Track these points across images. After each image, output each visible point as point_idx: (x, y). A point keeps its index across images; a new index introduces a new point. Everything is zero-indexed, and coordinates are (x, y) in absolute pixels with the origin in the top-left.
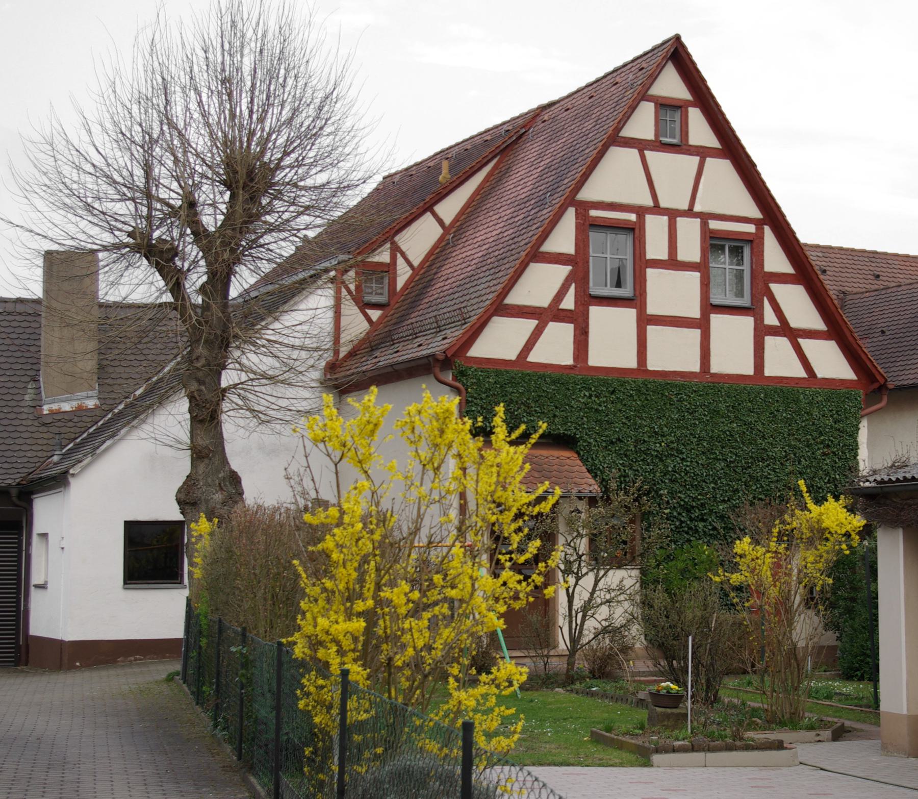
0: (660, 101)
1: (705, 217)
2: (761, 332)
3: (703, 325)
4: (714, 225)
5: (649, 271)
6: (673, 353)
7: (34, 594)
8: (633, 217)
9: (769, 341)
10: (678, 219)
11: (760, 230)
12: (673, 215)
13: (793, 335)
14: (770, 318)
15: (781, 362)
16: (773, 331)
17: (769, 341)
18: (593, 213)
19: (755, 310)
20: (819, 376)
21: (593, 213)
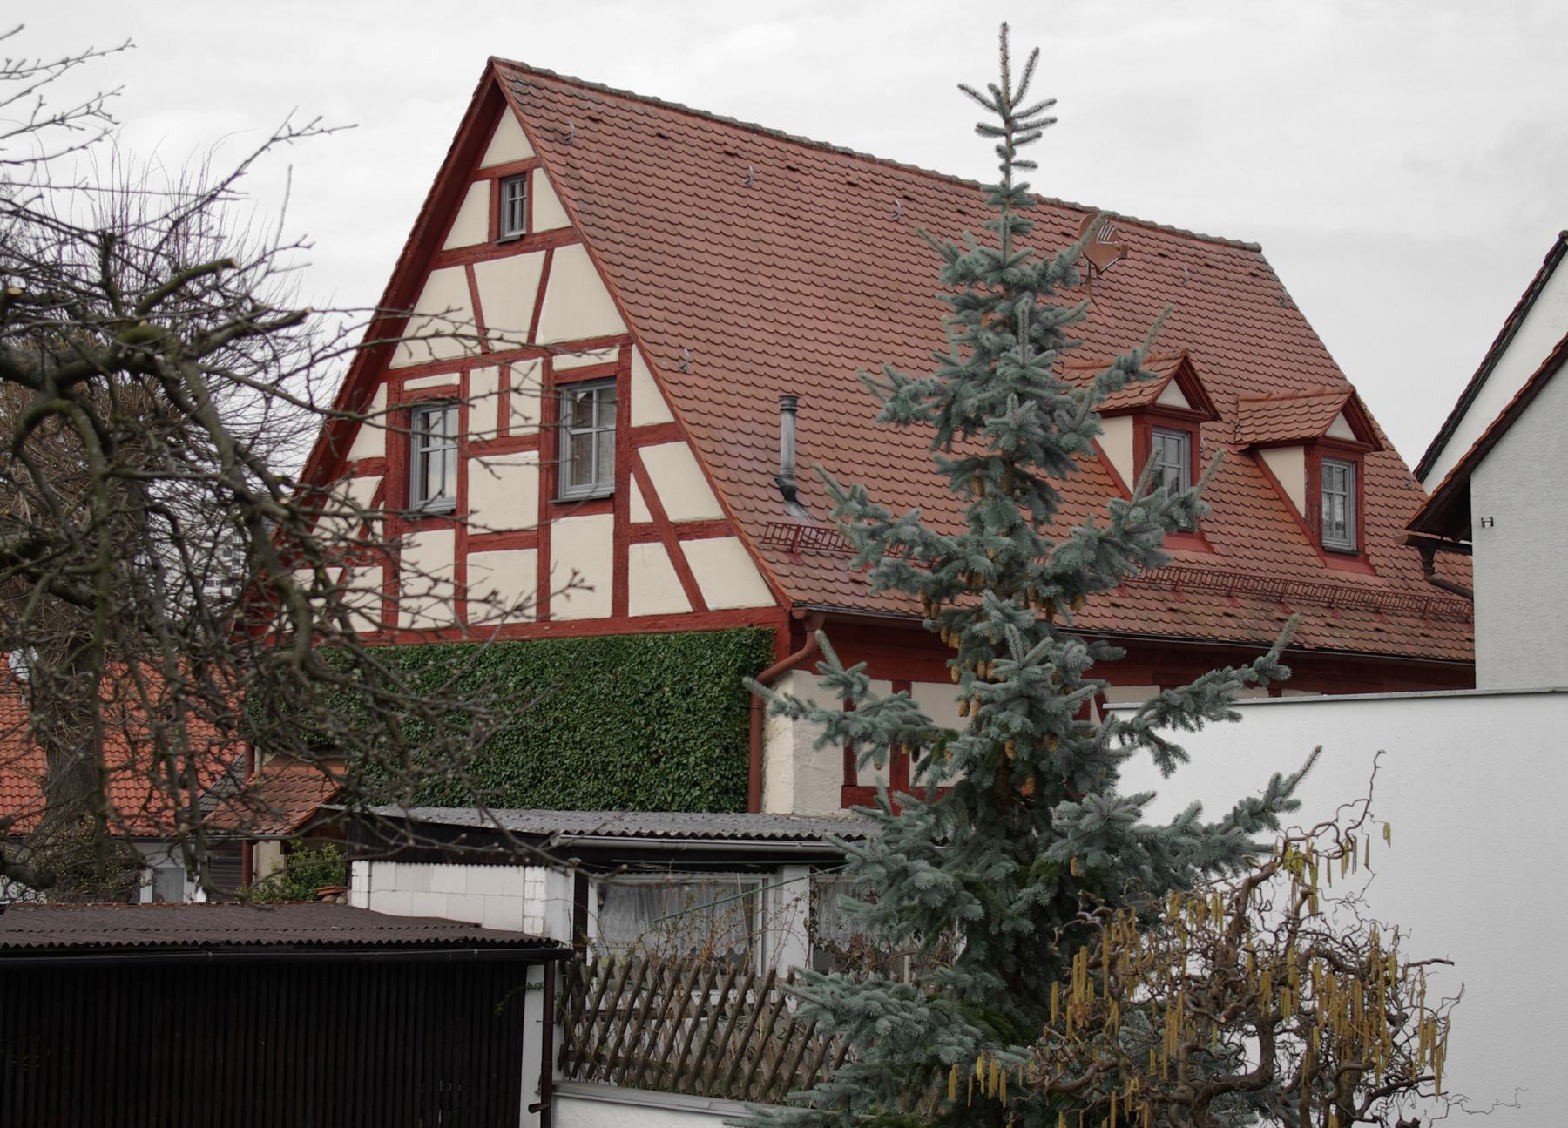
0: (499, 174)
1: (548, 352)
2: (626, 535)
3: (539, 539)
4: (562, 362)
5: (633, 611)
6: (505, 579)
7: (1055, 173)
8: (455, 378)
9: (637, 552)
10: (534, 551)
11: (625, 354)
12: (505, 361)
13: (670, 533)
14: (639, 512)
15: (655, 591)
16: (644, 534)
17: (637, 552)
18: (410, 385)
19: (615, 503)
20: (711, 606)
21: (410, 385)
